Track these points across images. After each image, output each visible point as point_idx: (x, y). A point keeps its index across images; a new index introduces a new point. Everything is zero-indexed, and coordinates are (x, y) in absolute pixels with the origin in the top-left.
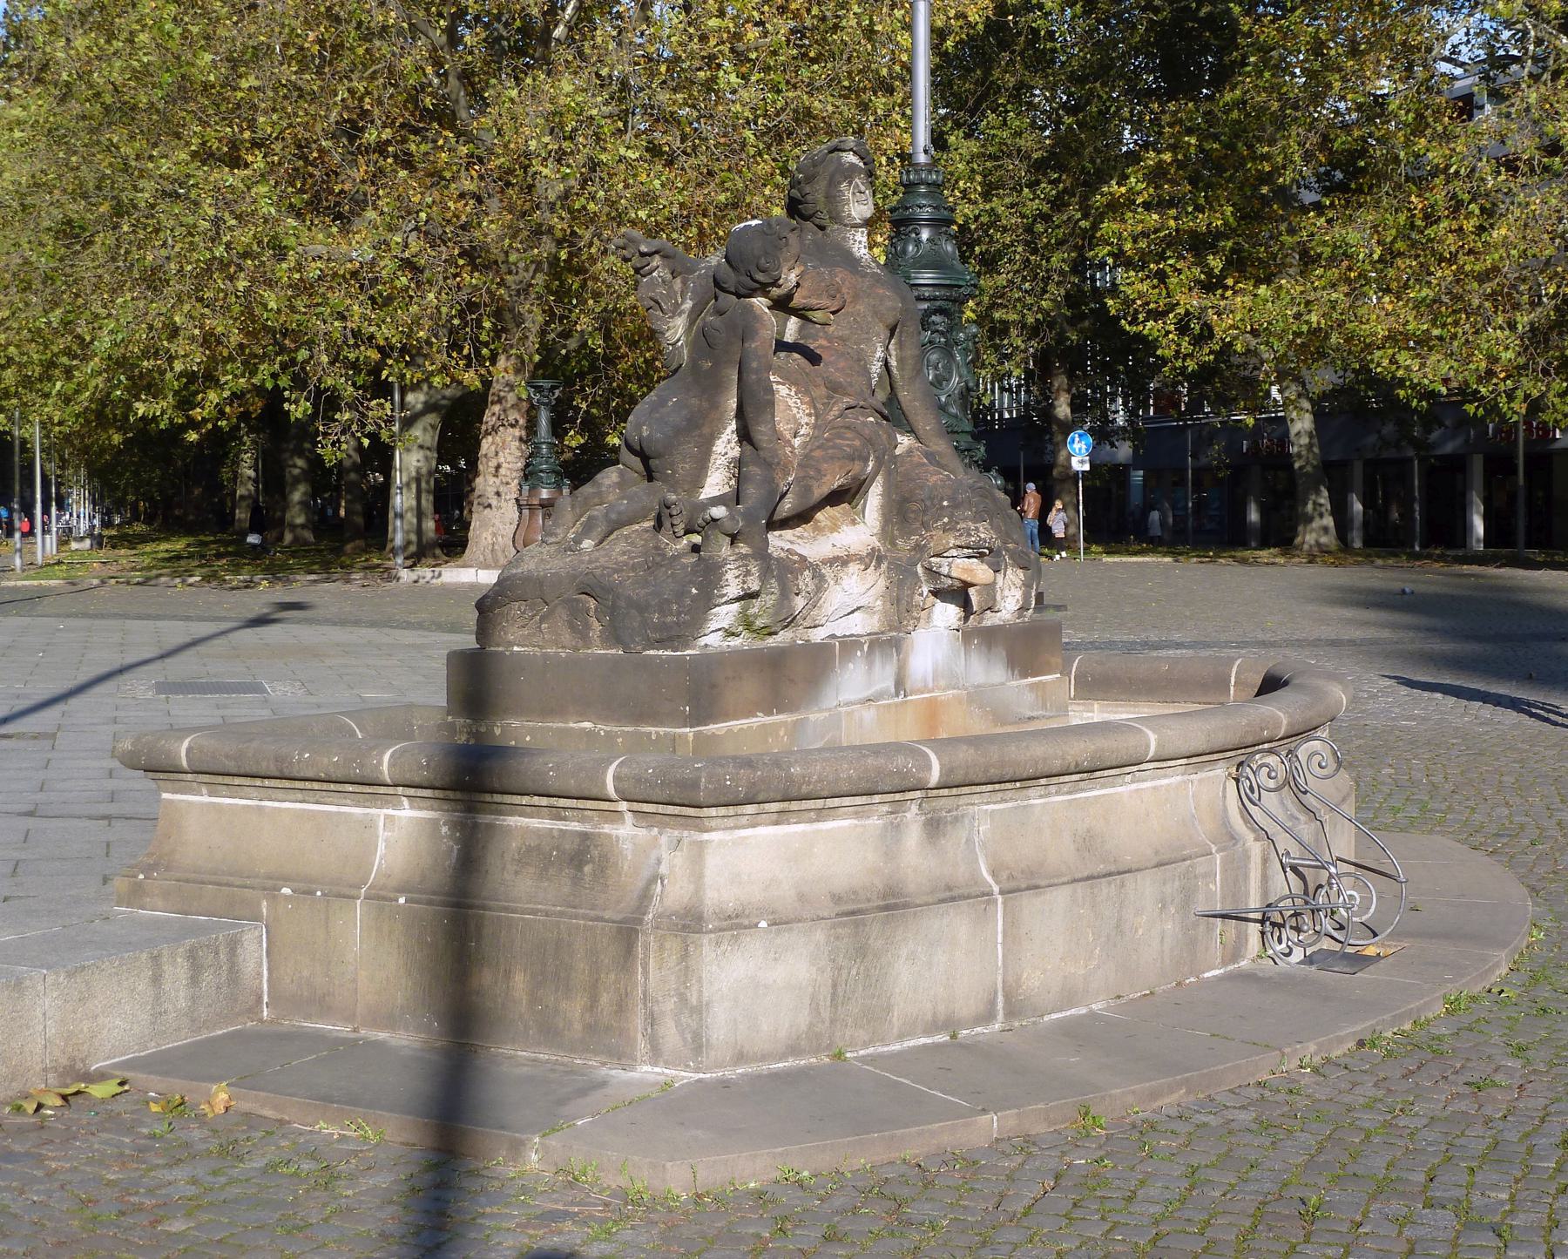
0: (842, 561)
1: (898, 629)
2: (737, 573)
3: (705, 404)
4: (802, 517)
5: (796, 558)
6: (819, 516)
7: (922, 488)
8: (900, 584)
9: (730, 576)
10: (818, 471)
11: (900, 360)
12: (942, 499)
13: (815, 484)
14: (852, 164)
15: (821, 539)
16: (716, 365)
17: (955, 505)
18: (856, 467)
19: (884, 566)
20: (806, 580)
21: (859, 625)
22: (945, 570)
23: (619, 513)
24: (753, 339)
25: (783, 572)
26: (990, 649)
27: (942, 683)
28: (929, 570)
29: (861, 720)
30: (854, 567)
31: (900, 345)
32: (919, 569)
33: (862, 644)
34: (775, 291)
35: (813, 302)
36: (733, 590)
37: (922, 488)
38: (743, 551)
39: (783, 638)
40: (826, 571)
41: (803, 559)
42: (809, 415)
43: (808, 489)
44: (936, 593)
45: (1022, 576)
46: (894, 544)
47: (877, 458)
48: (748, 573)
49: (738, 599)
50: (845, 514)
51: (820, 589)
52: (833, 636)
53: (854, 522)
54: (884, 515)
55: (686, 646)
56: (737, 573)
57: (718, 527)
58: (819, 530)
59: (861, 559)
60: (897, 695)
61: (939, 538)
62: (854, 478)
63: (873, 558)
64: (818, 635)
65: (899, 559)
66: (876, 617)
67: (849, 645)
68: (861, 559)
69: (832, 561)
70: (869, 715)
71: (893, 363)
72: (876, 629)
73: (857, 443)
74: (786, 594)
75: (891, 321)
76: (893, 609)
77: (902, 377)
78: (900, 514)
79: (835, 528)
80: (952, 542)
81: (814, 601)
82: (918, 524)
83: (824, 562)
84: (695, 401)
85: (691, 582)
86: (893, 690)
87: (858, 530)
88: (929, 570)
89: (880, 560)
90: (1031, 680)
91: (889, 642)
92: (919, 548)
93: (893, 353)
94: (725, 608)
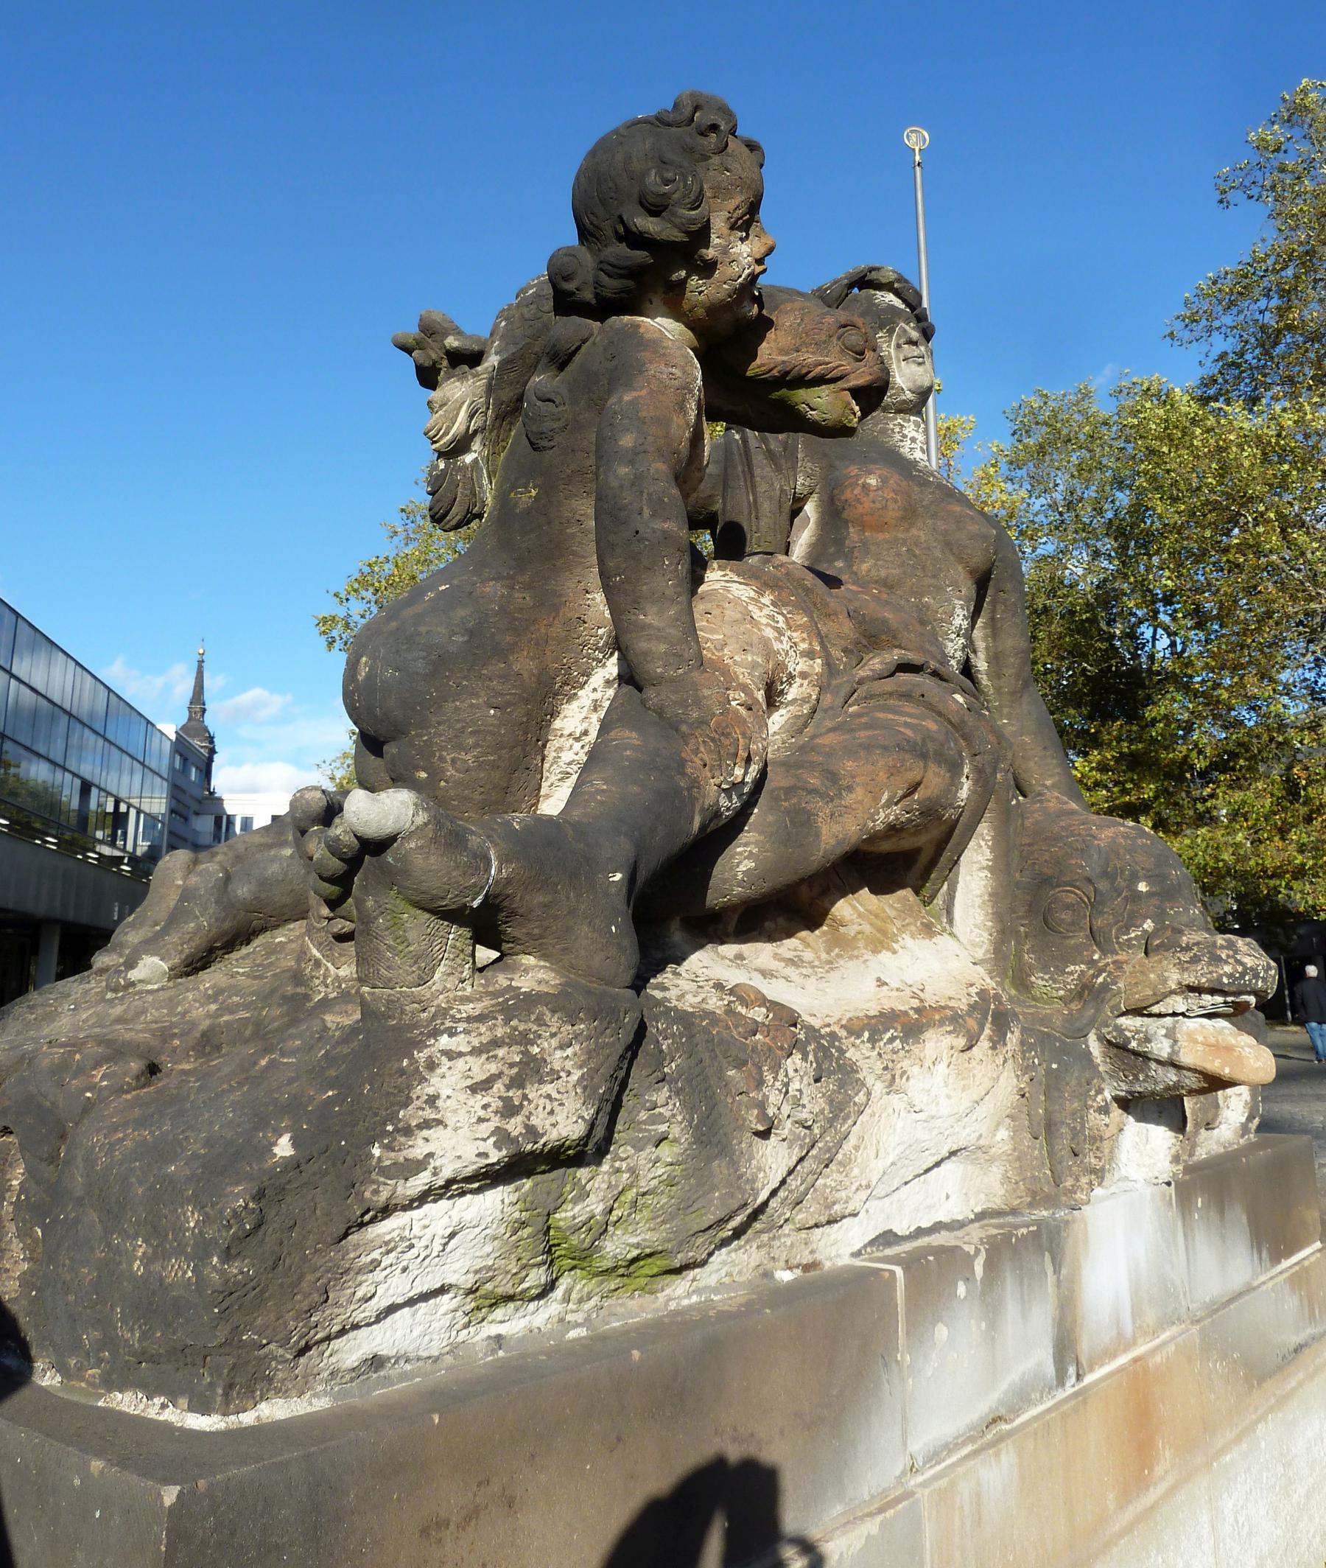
0: (906, 1025)
1: (1051, 1201)
2: (480, 1068)
3: (523, 598)
4: (789, 908)
5: (759, 1014)
6: (843, 908)
7: (1083, 852)
8: (1052, 1084)
9: (447, 1083)
10: (833, 777)
11: (995, 659)
12: (1135, 878)
13: (822, 810)
14: (892, 308)
15: (848, 967)
16: (548, 490)
17: (1166, 893)
18: (934, 780)
19: (1013, 1038)
20: (793, 1087)
21: (954, 1196)
22: (1161, 1048)
23: (262, 883)
24: (629, 386)
25: (723, 1063)
26: (1222, 1213)
27: (1151, 1317)
28: (1118, 1048)
29: (978, 1496)
30: (938, 1043)
31: (994, 630)
32: (1095, 1048)
33: (969, 1259)
34: (701, 291)
35: (808, 359)
36: (459, 1141)
37: (1083, 852)
38: (525, 983)
39: (727, 1273)
40: (859, 1053)
41: (786, 1018)
42: (810, 654)
43: (801, 822)
44: (1125, 1104)
45: (529, 960)
46: (1022, 983)
47: (979, 771)
48: (531, 1070)
49: (490, 1177)
50: (906, 910)
51: (841, 1109)
52: (888, 1238)
53: (928, 931)
54: (998, 916)
55: (248, 1381)
56: (480, 1068)
57: (391, 879)
58: (842, 944)
59: (954, 1020)
60: (1061, 1379)
61: (1133, 971)
62: (930, 812)
63: (987, 1019)
64: (840, 1247)
65: (1045, 1020)
66: (996, 1172)
67: (930, 1264)
68: (954, 1020)
69: (875, 1026)
70: (996, 1475)
71: (981, 664)
72: (997, 1203)
73: (932, 725)
74: (713, 1137)
75: (978, 560)
76: (1038, 1150)
77: (998, 690)
78: (1040, 911)
79: (881, 941)
80: (1175, 978)
81: (822, 1146)
82: (1081, 937)
83: (853, 1029)
84: (494, 589)
85: (294, 1108)
86: (1050, 1370)
87: (938, 951)
88: (1118, 1048)
89: (1002, 1023)
90: (1285, 1264)
91: (1028, 1240)
92: (1088, 993)
93: (981, 645)
94: (439, 1215)
